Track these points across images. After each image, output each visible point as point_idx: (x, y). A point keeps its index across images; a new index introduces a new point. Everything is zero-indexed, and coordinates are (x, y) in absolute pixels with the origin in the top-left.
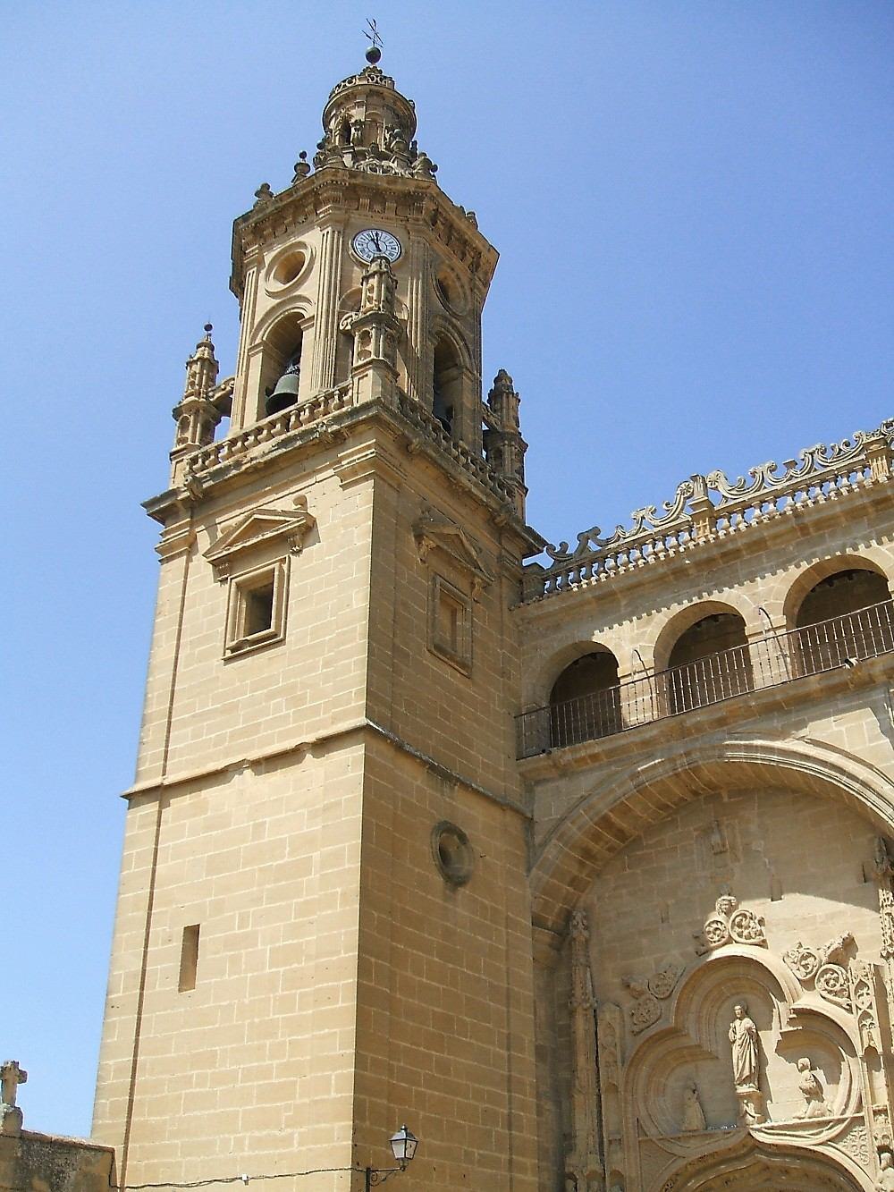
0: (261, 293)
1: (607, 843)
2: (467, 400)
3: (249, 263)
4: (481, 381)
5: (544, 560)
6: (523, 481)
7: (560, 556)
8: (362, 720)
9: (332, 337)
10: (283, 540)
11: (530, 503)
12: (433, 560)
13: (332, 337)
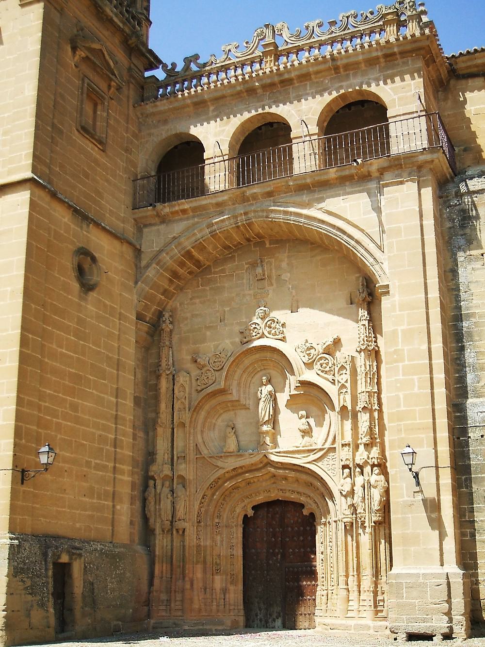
7: (171, 72)
12: (84, 67)
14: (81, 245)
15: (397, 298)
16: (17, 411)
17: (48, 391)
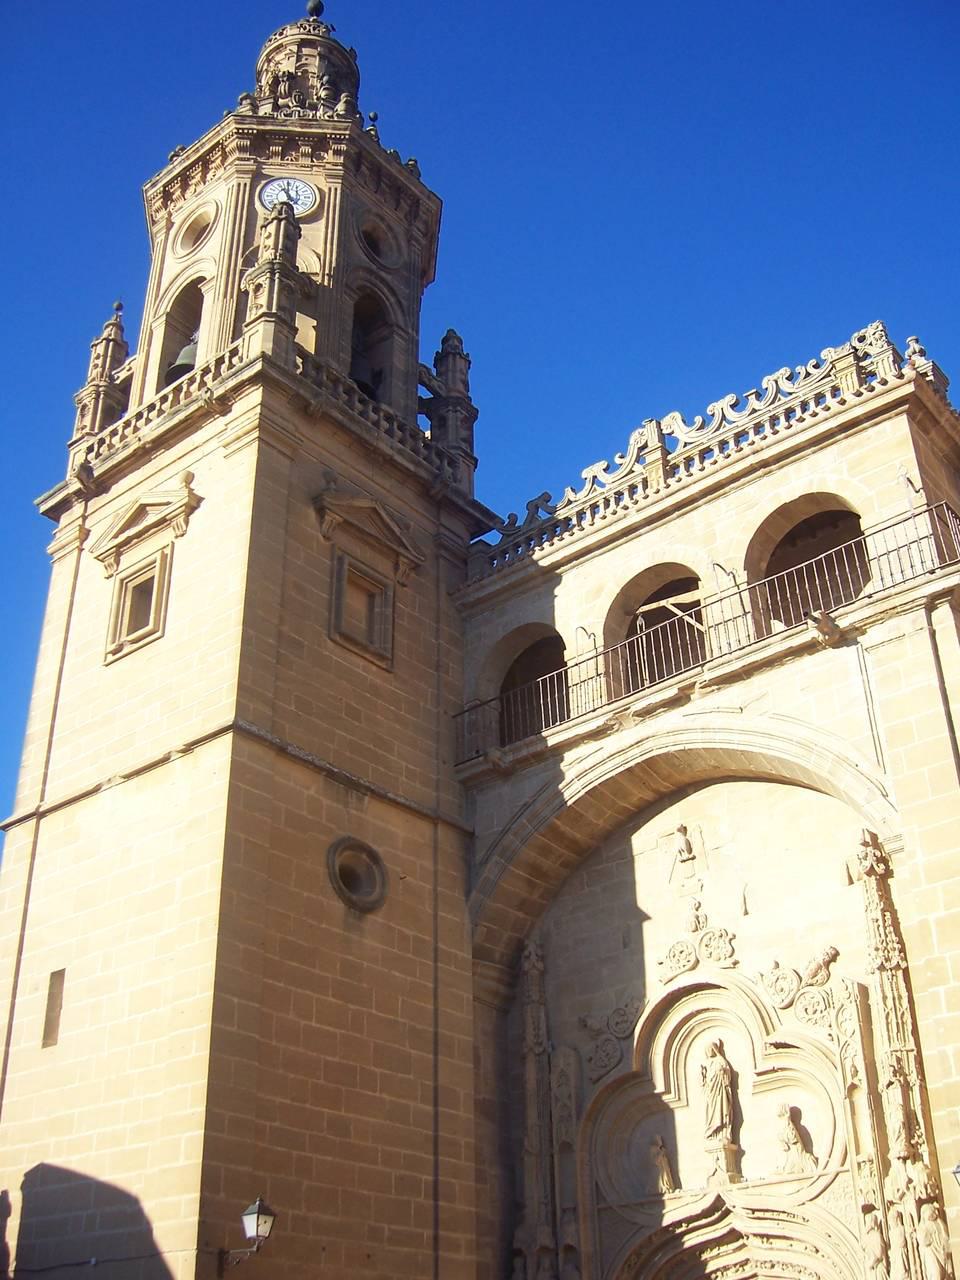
1: (560, 857)
2: (399, 362)
3: (157, 233)
4: (418, 341)
5: (493, 538)
6: (472, 450)
7: (510, 529)
9: (232, 297)
11: (478, 475)
12: (343, 540)
13: (232, 297)
14: (343, 834)
17: (279, 1100)
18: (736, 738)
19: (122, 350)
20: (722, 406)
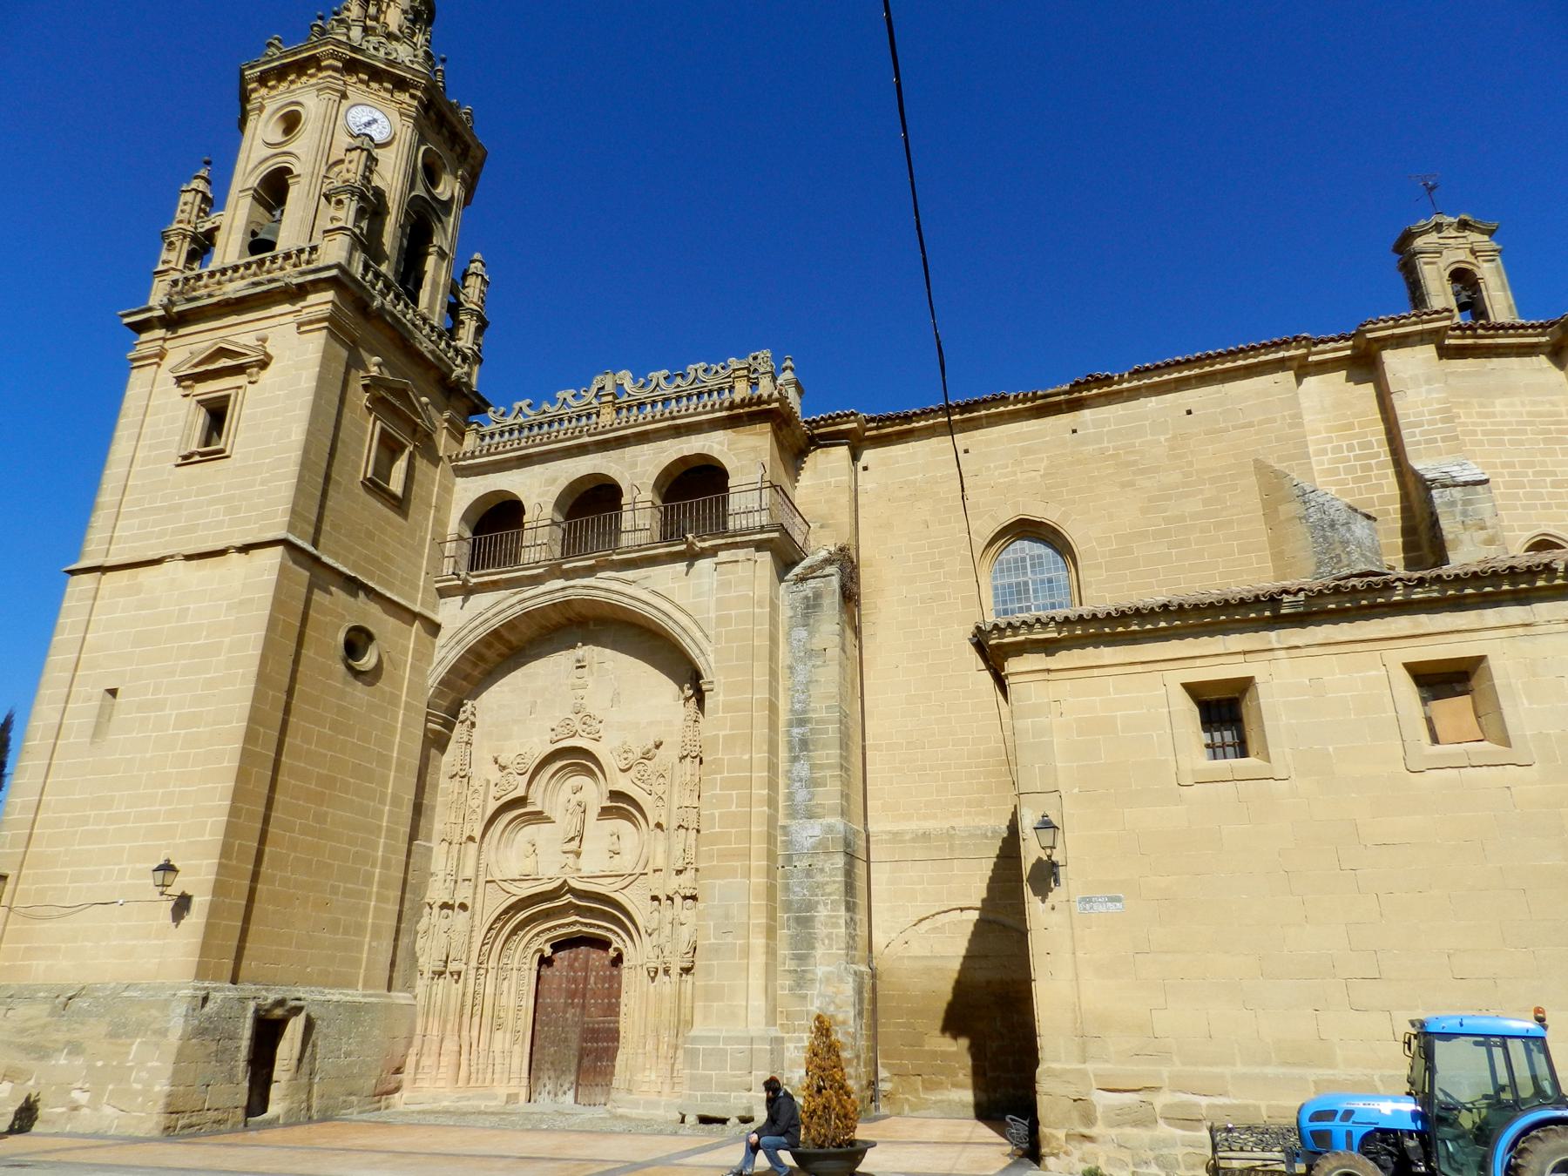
0: (258, 142)
8: (281, 534)
10: (239, 370)
15: (721, 697)
16: (229, 823)
18: (626, 600)
19: (210, 203)
20: (658, 375)
